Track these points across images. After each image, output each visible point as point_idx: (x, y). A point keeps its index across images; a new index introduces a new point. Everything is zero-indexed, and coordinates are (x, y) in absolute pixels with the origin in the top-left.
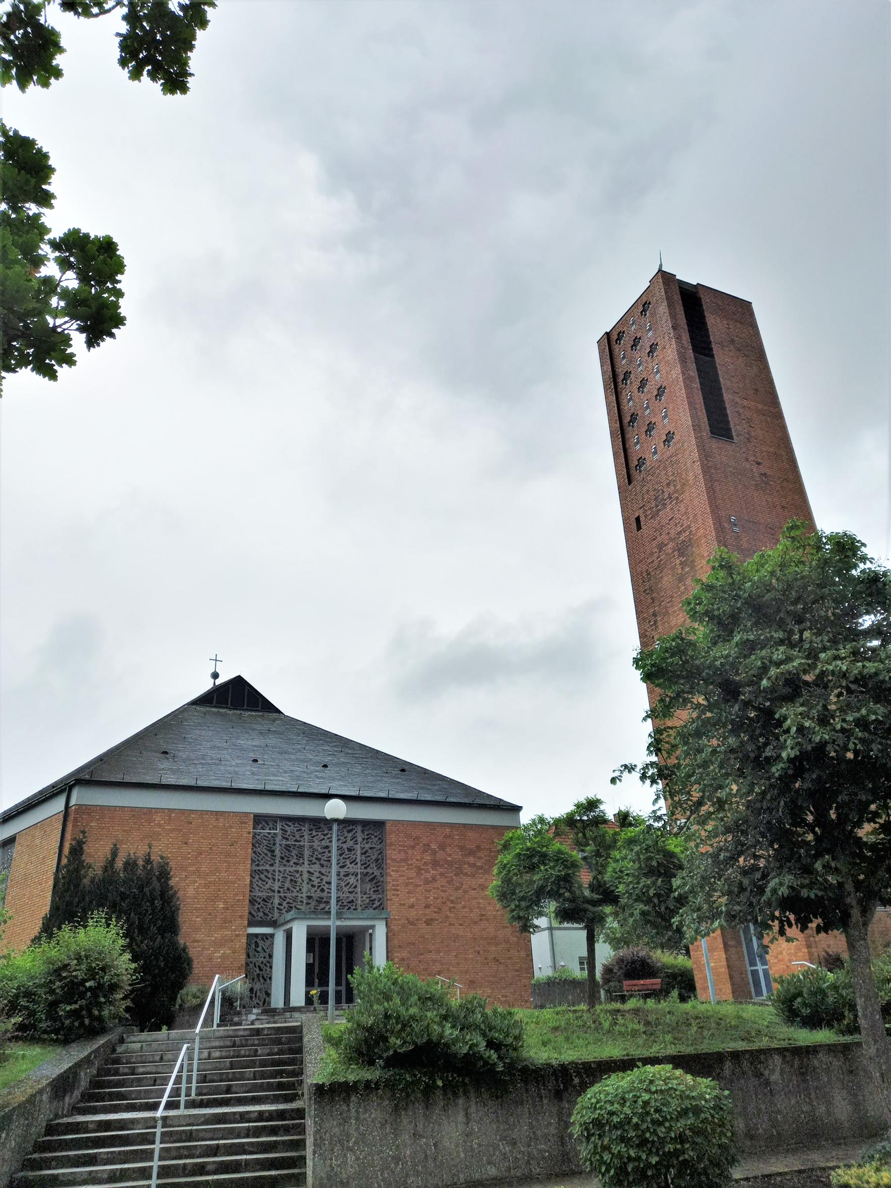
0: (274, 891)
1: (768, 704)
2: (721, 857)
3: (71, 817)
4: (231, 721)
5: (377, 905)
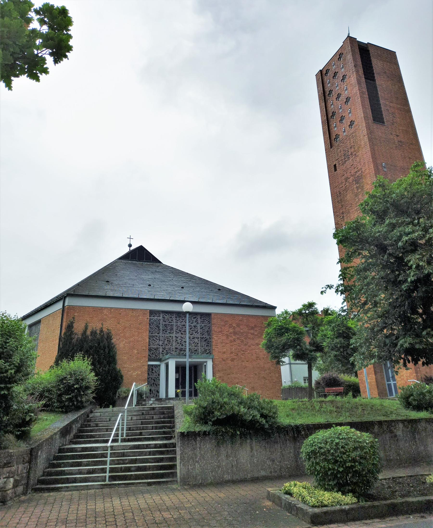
0: (160, 345)
1: (400, 255)
2: (376, 329)
3: (66, 311)
4: (138, 267)
5: (208, 352)
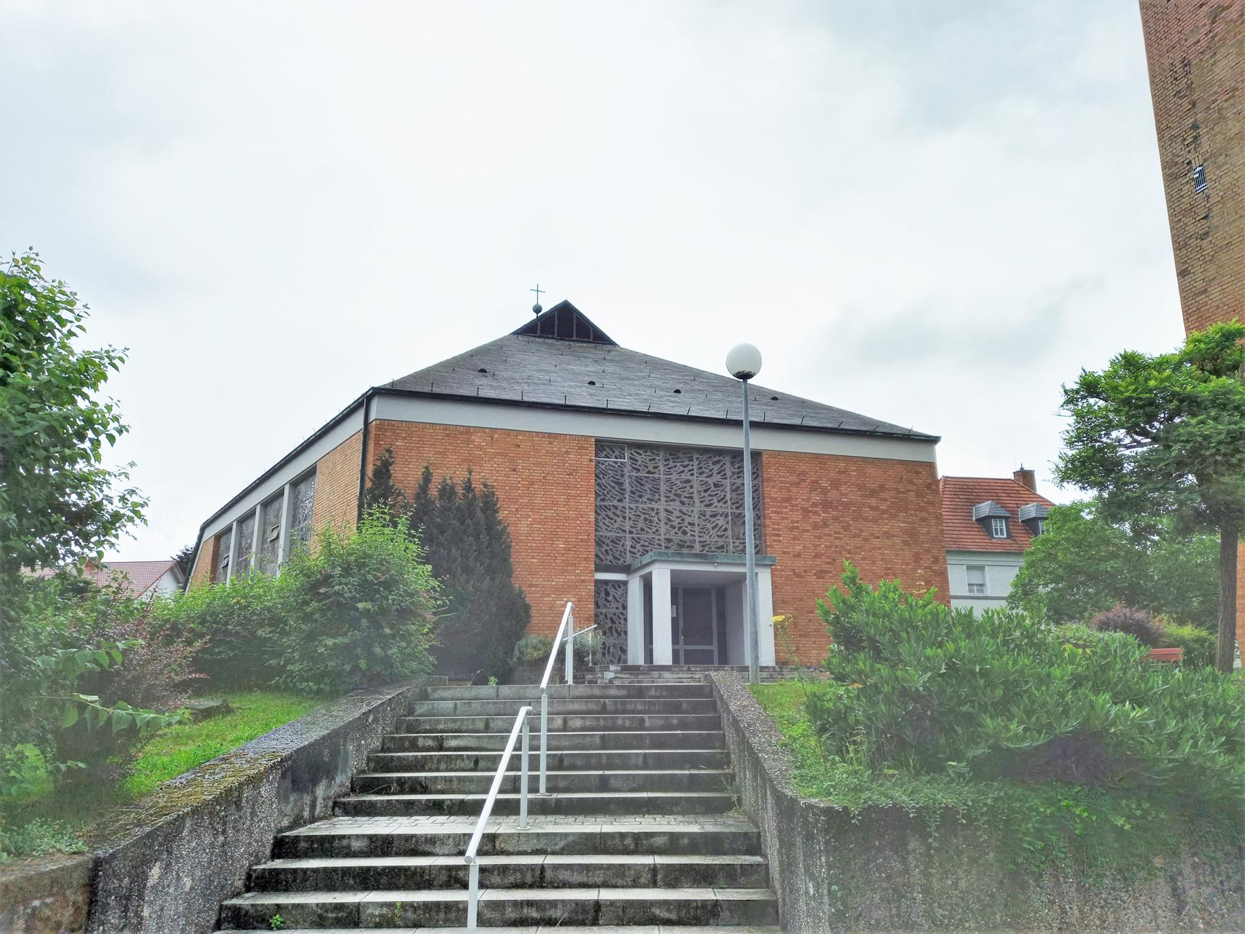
3: (372, 435)
